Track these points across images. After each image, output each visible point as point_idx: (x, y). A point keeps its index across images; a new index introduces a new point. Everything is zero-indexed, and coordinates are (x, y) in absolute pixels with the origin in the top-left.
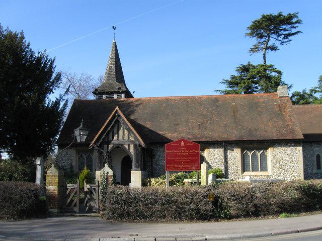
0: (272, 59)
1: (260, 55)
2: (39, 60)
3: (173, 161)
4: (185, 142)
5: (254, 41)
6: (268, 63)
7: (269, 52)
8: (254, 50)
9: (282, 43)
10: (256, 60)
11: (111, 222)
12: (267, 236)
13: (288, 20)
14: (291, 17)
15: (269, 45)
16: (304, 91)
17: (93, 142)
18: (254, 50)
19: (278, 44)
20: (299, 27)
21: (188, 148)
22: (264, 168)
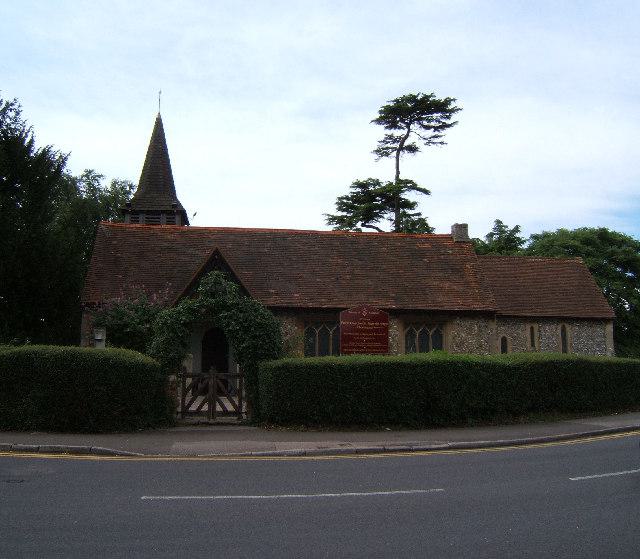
0: (411, 167)
1: (390, 161)
2: (613, 233)
3: (350, 339)
4: (370, 309)
5: (382, 131)
6: (401, 177)
7: (405, 156)
8: (382, 152)
9: (429, 143)
10: (384, 172)
11: (428, 322)
12: (509, 317)
13: (443, 107)
14: (448, 101)
15: (406, 144)
16: (517, 229)
17: (139, 357)
18: (382, 152)
19: (420, 144)
20: (454, 117)
21: (374, 319)
22: (439, 346)
